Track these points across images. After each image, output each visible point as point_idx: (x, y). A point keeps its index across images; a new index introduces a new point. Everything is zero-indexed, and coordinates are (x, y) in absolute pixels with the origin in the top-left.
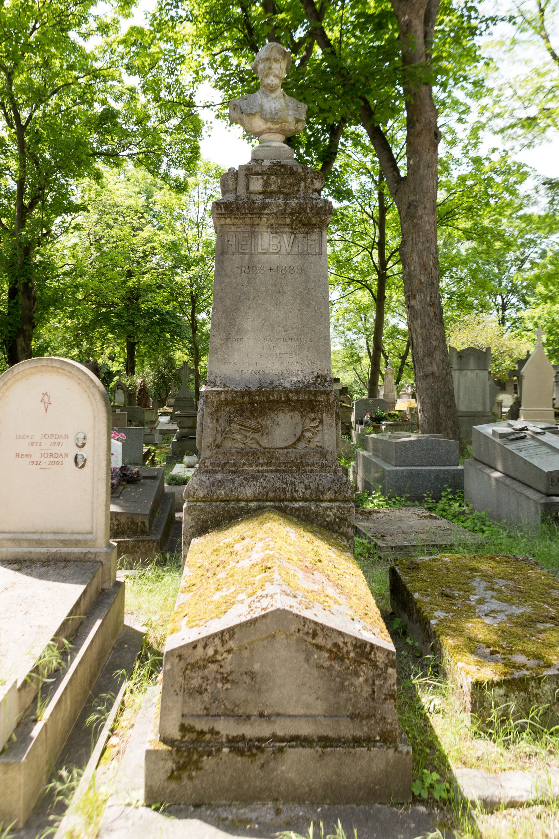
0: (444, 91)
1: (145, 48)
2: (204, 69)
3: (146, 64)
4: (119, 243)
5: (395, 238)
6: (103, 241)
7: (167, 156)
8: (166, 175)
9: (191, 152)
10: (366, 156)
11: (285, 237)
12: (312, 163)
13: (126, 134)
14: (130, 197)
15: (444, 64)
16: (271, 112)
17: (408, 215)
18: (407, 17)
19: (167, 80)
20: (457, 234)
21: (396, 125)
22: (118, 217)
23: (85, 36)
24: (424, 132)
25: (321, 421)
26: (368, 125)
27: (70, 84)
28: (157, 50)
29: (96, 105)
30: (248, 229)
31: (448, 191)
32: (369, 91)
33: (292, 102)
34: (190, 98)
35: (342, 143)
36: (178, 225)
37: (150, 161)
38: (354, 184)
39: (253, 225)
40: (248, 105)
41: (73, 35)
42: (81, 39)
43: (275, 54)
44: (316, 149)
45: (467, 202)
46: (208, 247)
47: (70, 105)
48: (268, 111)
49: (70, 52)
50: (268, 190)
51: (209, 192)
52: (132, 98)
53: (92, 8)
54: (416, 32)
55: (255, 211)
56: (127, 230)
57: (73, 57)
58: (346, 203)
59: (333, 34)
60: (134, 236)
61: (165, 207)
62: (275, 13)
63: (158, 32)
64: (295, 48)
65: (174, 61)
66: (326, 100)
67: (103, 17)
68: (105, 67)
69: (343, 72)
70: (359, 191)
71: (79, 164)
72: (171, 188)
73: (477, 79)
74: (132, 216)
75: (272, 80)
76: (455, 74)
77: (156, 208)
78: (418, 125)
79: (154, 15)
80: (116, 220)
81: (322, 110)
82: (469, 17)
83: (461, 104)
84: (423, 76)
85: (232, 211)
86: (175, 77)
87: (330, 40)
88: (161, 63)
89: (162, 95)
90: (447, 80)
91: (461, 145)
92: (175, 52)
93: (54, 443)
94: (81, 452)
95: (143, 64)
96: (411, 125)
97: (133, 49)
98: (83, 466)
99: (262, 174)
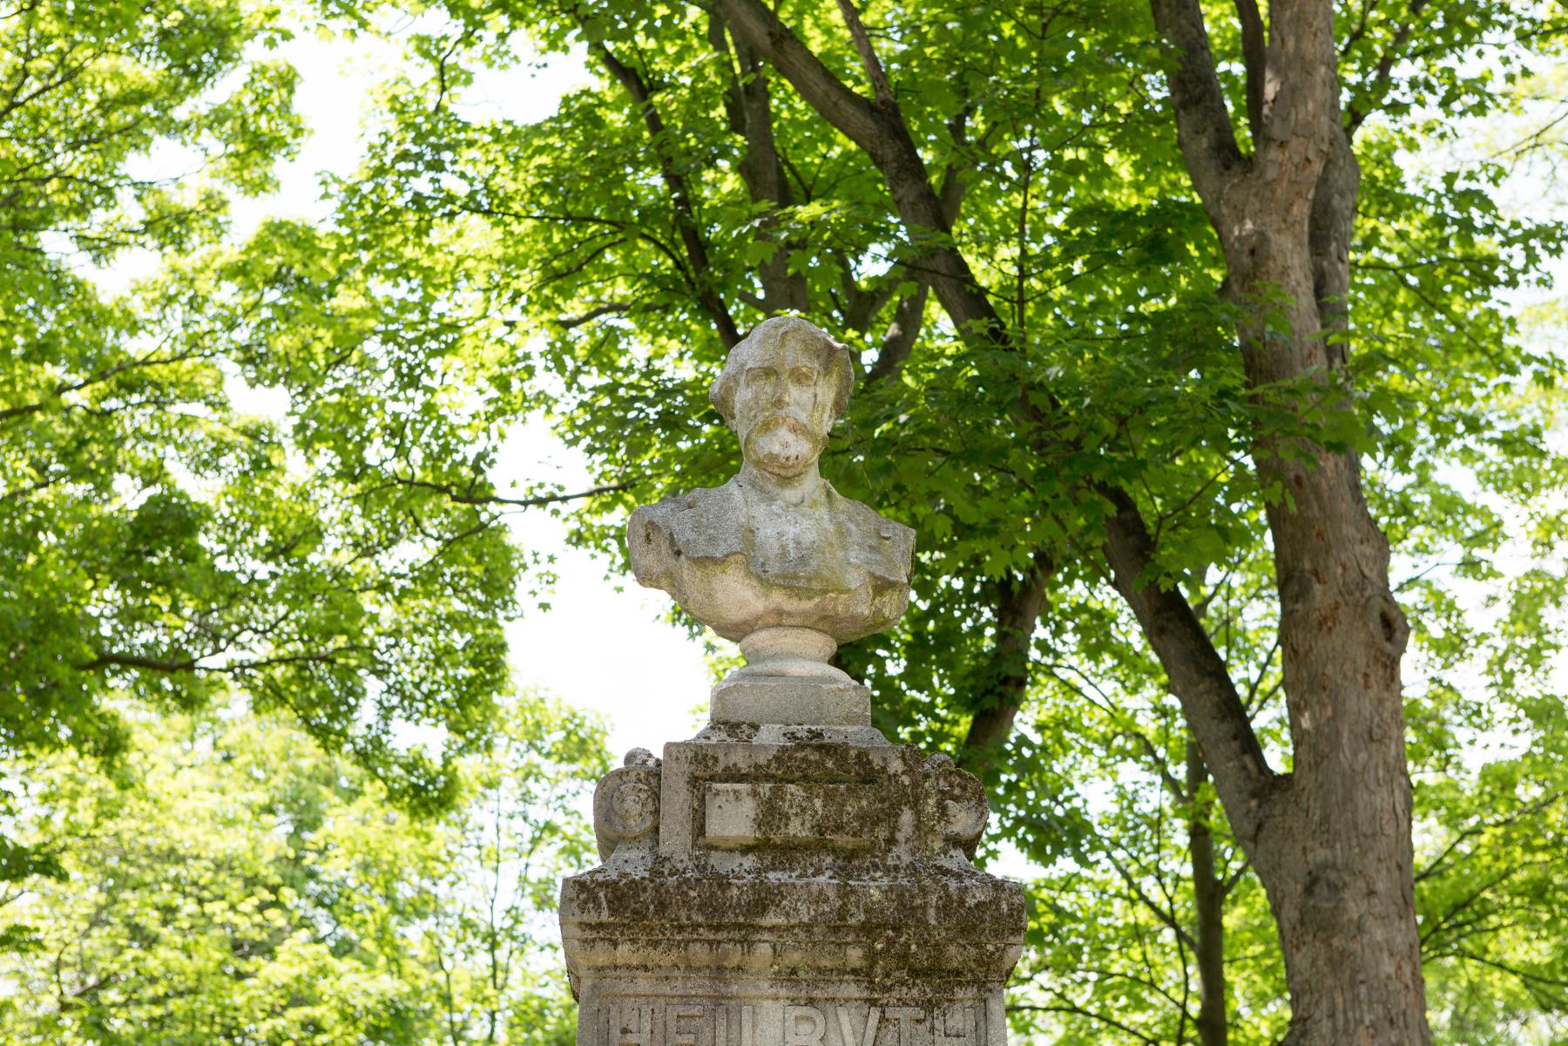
0: (1405, 469)
1: (316, 295)
2: (530, 371)
3: (318, 348)
4: (175, 1005)
5: (1263, 998)
6: (112, 996)
7: (380, 674)
8: (377, 743)
9: (475, 663)
10: (1134, 691)
11: (847, 1020)
12: (929, 710)
13: (228, 591)
14: (230, 823)
15: (1393, 378)
16: (784, 553)
17: (1312, 923)
18: (1249, 225)
19: (391, 407)
20: (1501, 986)
21: (1236, 579)
22: (178, 900)
23: (100, 248)
24: (1342, 614)
26: (1138, 586)
27: (32, 409)
28: (360, 303)
29: (121, 482)
30: (700, 985)
31: (1452, 821)
32: (1136, 468)
33: (856, 517)
34: (477, 469)
35: (1044, 647)
36: (414, 935)
37: (313, 691)
38: (1095, 792)
39: (719, 972)
40: (697, 528)
41: (55, 243)
42: (87, 257)
43: (794, 355)
44: (948, 664)
45: (1526, 866)
46: (529, 1027)
47: (26, 484)
48: (773, 548)
49: (42, 299)
50: (777, 839)
51: (539, 813)
52: (260, 465)
53: (132, 156)
54: (1284, 272)
55: (730, 918)
56: (210, 952)
57: (50, 316)
58: (1066, 865)
59: (990, 270)
60: (240, 976)
61: (365, 867)
62: (786, 198)
63: (366, 246)
64: (861, 308)
65: (419, 341)
66: (977, 492)
67: (170, 189)
68: (166, 352)
69: (1036, 398)
70: (1119, 821)
71: (41, 699)
72: (393, 796)
73: (1513, 425)
74: (234, 896)
75: (786, 444)
76: (1433, 408)
77: (336, 868)
78: (1318, 588)
79: (353, 191)
80: (168, 913)
81: (964, 530)
82: (1467, 226)
83: (1468, 510)
84: (1323, 421)
85: (639, 915)
86: (420, 397)
87: (984, 291)
88: (372, 346)
89: (372, 455)
90: (1411, 429)
91: (1482, 656)
92: (425, 312)
95: (306, 347)
96: (1294, 588)
97: (273, 295)
99: (755, 776)
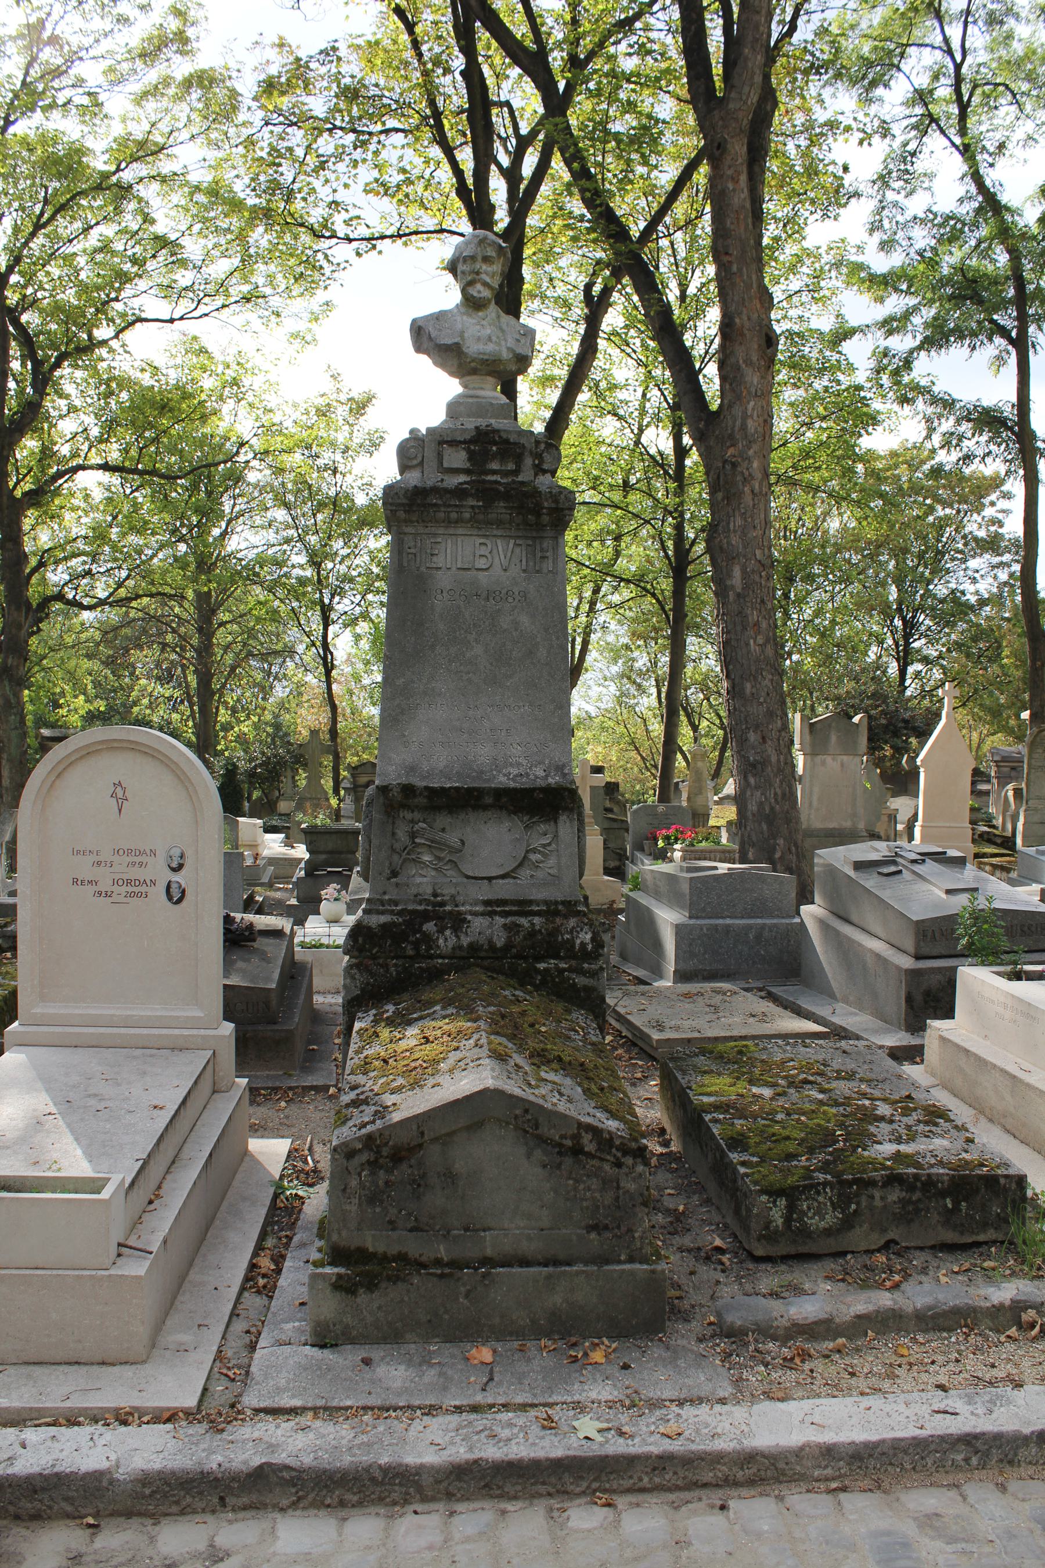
25: (556, 836)
93: (134, 864)
94: (176, 878)
98: (180, 901)
